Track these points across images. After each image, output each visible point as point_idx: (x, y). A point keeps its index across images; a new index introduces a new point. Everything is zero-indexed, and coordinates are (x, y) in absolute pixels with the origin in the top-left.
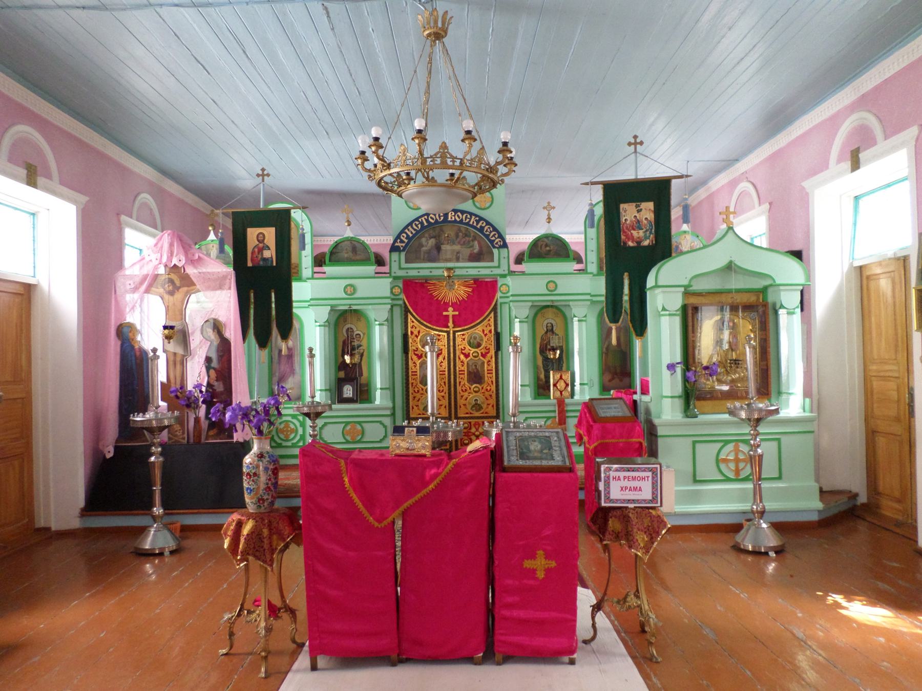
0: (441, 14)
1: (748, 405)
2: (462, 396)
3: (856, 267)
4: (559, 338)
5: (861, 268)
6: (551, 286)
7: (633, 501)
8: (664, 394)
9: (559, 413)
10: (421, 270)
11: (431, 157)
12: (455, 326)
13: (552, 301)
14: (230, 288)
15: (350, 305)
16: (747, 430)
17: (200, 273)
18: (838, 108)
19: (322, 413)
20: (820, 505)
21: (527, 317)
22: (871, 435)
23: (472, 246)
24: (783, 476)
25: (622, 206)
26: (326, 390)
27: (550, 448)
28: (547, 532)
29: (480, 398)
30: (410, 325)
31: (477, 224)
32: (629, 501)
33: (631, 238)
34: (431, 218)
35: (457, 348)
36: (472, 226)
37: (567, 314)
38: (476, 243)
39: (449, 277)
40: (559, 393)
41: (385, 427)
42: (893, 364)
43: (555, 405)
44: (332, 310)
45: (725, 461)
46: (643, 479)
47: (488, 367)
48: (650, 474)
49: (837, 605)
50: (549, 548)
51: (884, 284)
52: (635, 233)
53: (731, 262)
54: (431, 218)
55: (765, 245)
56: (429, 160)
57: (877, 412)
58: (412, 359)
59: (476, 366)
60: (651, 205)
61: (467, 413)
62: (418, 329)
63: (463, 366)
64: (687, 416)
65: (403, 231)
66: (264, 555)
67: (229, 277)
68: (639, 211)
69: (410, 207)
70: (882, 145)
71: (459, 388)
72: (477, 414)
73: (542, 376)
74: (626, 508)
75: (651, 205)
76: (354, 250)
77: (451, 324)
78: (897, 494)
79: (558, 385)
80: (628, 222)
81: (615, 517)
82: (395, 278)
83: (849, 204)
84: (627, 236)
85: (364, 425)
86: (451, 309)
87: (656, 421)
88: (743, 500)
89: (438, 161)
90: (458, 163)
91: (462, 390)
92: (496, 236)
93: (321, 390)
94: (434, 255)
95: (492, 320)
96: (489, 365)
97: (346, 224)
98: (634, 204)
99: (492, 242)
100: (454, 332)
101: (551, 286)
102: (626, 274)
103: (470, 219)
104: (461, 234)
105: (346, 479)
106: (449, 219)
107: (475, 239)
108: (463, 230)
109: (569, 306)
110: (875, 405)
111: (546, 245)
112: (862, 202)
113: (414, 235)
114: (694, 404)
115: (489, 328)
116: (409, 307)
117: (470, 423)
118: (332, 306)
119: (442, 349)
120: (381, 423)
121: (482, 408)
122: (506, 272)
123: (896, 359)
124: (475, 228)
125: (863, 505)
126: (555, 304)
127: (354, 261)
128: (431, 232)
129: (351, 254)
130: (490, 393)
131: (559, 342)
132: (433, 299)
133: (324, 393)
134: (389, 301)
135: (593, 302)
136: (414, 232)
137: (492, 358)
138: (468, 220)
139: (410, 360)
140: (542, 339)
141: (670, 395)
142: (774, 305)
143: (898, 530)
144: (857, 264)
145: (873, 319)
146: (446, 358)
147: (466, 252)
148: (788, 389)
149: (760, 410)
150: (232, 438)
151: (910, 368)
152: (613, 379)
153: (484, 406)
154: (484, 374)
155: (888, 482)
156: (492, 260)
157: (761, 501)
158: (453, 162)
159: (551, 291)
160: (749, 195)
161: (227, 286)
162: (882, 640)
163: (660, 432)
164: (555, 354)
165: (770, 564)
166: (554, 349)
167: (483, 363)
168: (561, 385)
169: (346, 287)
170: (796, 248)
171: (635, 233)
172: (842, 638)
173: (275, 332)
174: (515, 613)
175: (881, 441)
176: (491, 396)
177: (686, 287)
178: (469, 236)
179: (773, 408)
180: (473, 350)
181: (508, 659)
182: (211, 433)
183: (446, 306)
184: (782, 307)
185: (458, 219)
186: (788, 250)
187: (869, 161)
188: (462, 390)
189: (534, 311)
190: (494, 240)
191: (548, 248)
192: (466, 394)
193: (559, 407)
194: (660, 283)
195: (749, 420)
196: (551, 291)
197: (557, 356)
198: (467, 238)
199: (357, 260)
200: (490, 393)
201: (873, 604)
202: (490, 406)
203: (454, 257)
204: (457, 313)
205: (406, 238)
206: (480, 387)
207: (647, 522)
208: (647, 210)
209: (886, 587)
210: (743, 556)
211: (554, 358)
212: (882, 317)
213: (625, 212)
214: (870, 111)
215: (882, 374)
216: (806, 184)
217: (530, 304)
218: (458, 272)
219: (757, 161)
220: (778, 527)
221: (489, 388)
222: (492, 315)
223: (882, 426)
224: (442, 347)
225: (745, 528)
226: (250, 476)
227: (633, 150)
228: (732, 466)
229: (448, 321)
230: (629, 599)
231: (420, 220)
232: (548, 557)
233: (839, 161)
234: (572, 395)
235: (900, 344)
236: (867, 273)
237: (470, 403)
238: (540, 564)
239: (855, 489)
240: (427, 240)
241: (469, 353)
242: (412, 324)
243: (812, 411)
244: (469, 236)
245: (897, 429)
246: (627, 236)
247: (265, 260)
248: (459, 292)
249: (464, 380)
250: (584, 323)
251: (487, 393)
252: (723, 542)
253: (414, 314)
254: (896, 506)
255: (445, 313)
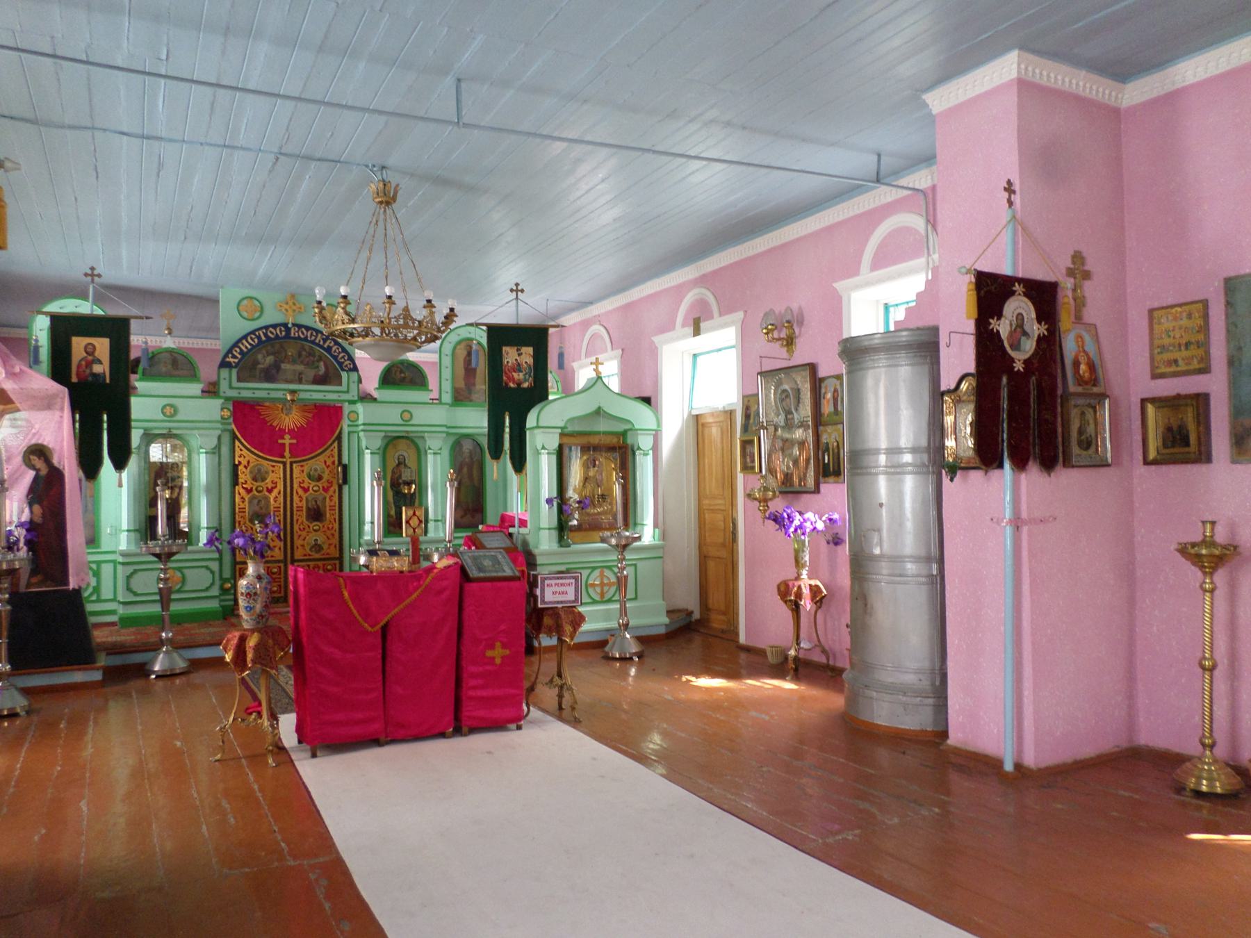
0: (393, 186)
1: (618, 533)
2: (300, 536)
3: (693, 416)
4: (411, 472)
5: (697, 416)
6: (407, 416)
7: (562, 602)
8: (542, 526)
9: (413, 552)
10: (255, 390)
11: (395, 317)
12: (293, 454)
13: (407, 432)
14: (62, 409)
15: (170, 429)
16: (614, 557)
17: (22, 389)
18: (685, 279)
19: (174, 554)
20: (666, 620)
21: (379, 449)
22: (703, 559)
23: (318, 367)
24: (639, 597)
25: (504, 348)
26: (135, 530)
27: (499, 563)
28: (503, 627)
29: (321, 539)
30: (238, 452)
31: (324, 342)
32: (558, 602)
33: (513, 380)
34: (271, 332)
35: (295, 481)
36: (318, 345)
37: (421, 445)
38: (322, 364)
39: (293, 401)
40: (412, 530)
41: (212, 572)
42: (720, 499)
43: (408, 543)
44: (144, 434)
45: (593, 585)
46: (569, 584)
47: (330, 503)
48: (573, 581)
49: (689, 681)
50: (505, 640)
51: (715, 432)
52: (515, 375)
53: (599, 408)
54: (271, 332)
55: (617, 391)
56: (393, 320)
57: (708, 540)
58: (239, 494)
59: (316, 501)
60: (530, 350)
61: (305, 555)
62: (247, 459)
63: (301, 501)
64: (561, 546)
65: (236, 345)
66: (271, 662)
67: (61, 395)
68: (519, 355)
69: (244, 318)
70: (717, 320)
71: (296, 527)
72: (317, 556)
73: (393, 512)
74: (557, 607)
75: (530, 350)
76: (175, 362)
77: (287, 454)
78: (723, 608)
79: (411, 522)
80: (510, 364)
81: (549, 615)
82: (227, 399)
83: (688, 361)
84: (508, 378)
85: (185, 571)
86: (287, 437)
87: (536, 551)
88: (607, 619)
89: (401, 322)
90: (416, 324)
91: (300, 529)
92: (346, 358)
93: (128, 531)
94: (270, 375)
95: (336, 450)
96: (331, 500)
97: (166, 332)
98: (516, 348)
99: (340, 364)
100: (291, 463)
101: (407, 416)
102: (507, 413)
103: (316, 337)
104: (304, 353)
105: (346, 594)
106: (292, 335)
107: (320, 359)
108: (307, 348)
109: (423, 437)
110: (707, 535)
111: (401, 372)
112: (699, 359)
113: (249, 351)
114: (568, 535)
115: (332, 459)
116: (237, 433)
117: (309, 566)
118: (145, 429)
119: (276, 483)
120: (207, 568)
121: (322, 548)
122: (356, 398)
123: (723, 495)
124: (321, 347)
125: (696, 621)
126: (411, 435)
127: (175, 376)
128: (269, 348)
129: (170, 367)
130: (333, 532)
131: (411, 476)
132: (266, 424)
133: (132, 534)
134: (219, 425)
135: (448, 434)
136: (249, 347)
137: (334, 492)
138: (313, 338)
139: (237, 496)
140: (393, 472)
141: (547, 527)
142: (632, 447)
143: (724, 636)
144: (695, 412)
145: (706, 461)
146: (282, 493)
147: (310, 373)
148: (643, 520)
149: (627, 537)
150: (67, 583)
151: (734, 502)
152: (466, 514)
153: (325, 547)
154: (325, 511)
155: (716, 600)
156: (340, 384)
157: (626, 615)
158: (413, 323)
159: (406, 421)
160: (602, 338)
161: (58, 406)
162: (722, 693)
163: (539, 560)
164: (410, 489)
165: (630, 670)
166: (409, 484)
167: (325, 498)
168: (414, 522)
169: (164, 407)
170: (645, 394)
171: (515, 375)
172: (697, 697)
173: (107, 464)
174: (479, 693)
175: (711, 565)
176: (333, 535)
177: (562, 428)
178: (314, 356)
179: (637, 535)
180: (314, 483)
181: (473, 730)
182: (34, 580)
183: (282, 433)
184: (639, 448)
185: (302, 336)
186: (637, 396)
187: (708, 330)
188: (300, 529)
189: (386, 441)
190: (343, 363)
191: (403, 375)
192: (304, 533)
193: (413, 545)
194: (541, 424)
195: (617, 545)
196: (406, 421)
197: (413, 490)
198: (312, 358)
199: (179, 376)
200: (333, 532)
201: (713, 677)
202: (332, 547)
203: (297, 378)
204: (294, 441)
205: (239, 354)
206: (321, 525)
207: (571, 617)
208: (527, 355)
209: (721, 669)
210: (611, 662)
211: (409, 493)
212: (714, 457)
213: (507, 354)
214: (708, 289)
215: (712, 508)
216: (657, 339)
217: (383, 434)
218: (303, 396)
219: (610, 308)
220: (641, 640)
221: (330, 526)
222: (336, 444)
223: (713, 552)
224: (276, 480)
225: (610, 643)
226: (250, 596)
227: (515, 296)
228: (598, 590)
229: (284, 450)
230: (554, 680)
231: (257, 333)
232: (504, 646)
233: (684, 325)
234: (426, 532)
235: (726, 483)
236: (702, 421)
237: (308, 544)
238: (498, 653)
239: (690, 608)
240: (264, 357)
241: (309, 487)
242: (240, 452)
243: (659, 540)
244: (314, 356)
245: (724, 553)
246: (508, 378)
247: (95, 375)
248: (292, 419)
249: (301, 517)
250: (438, 456)
251: (329, 533)
252: (598, 653)
253: (243, 441)
254: (723, 618)
255: (280, 441)
